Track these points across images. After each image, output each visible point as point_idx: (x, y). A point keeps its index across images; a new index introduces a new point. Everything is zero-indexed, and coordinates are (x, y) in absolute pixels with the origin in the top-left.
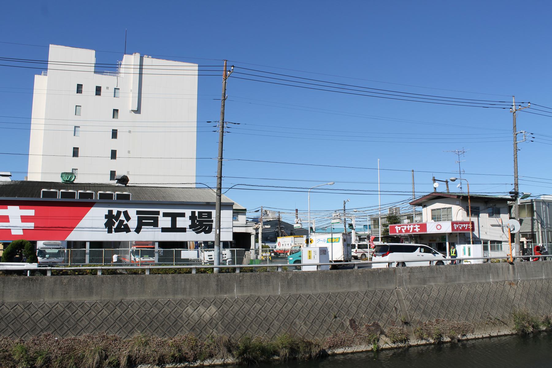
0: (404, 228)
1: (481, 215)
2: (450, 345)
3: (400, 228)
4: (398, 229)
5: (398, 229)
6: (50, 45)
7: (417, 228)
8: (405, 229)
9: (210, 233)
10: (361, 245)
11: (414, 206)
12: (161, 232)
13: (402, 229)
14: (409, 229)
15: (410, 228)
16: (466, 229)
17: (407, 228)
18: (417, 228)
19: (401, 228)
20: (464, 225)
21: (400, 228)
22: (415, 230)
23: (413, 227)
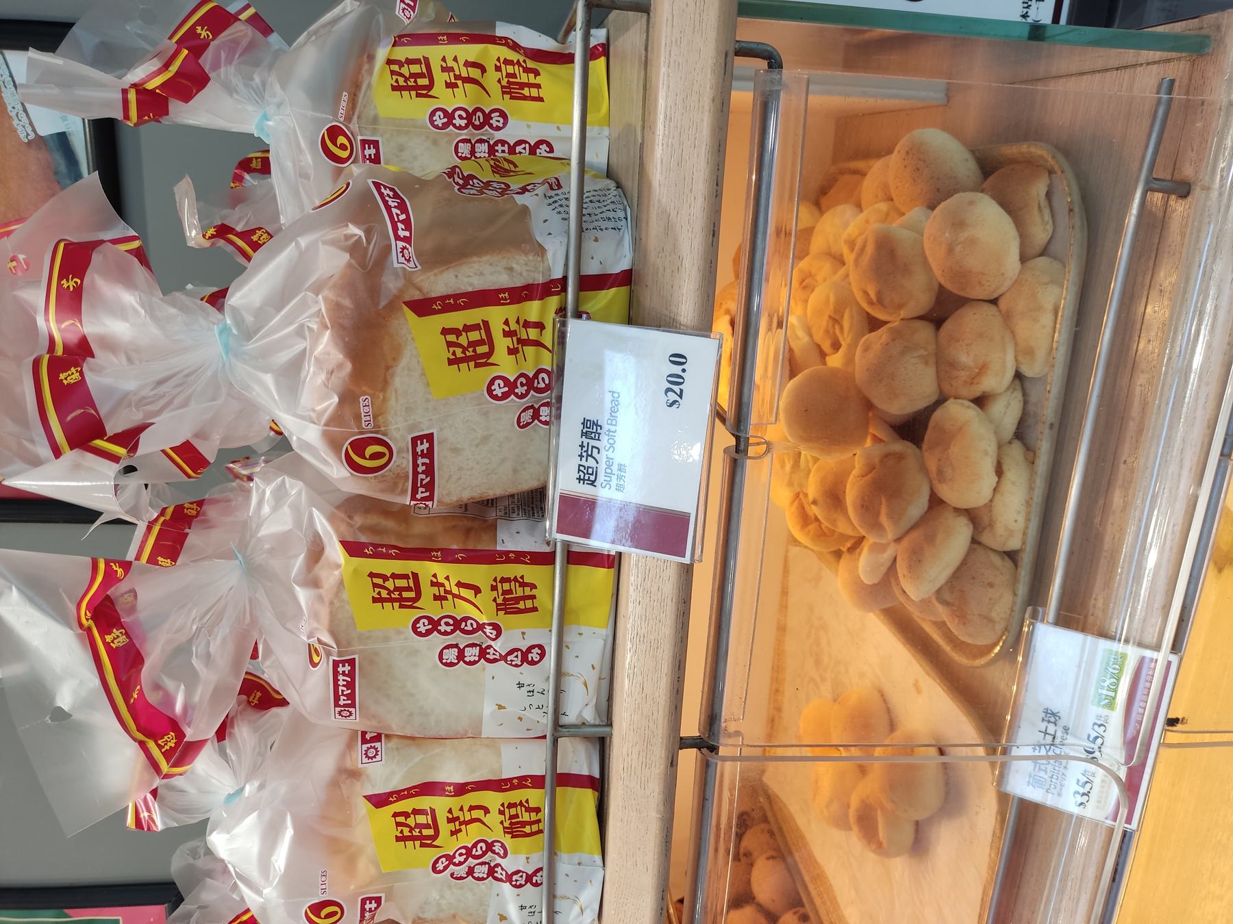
0: (422, 480)
1: (346, 257)
3: (342, 698)
4: (344, 700)
5: (344, 700)
6: (497, 23)
7: (371, 906)
9: (420, 599)
10: (856, 348)
12: (599, 502)
14: (345, 683)
15: (344, 680)
16: (349, 680)
17: (423, 472)
18: (371, 906)
19: (343, 695)
20: (341, 683)
21: (342, 698)
22: (347, 672)
23: (368, 161)
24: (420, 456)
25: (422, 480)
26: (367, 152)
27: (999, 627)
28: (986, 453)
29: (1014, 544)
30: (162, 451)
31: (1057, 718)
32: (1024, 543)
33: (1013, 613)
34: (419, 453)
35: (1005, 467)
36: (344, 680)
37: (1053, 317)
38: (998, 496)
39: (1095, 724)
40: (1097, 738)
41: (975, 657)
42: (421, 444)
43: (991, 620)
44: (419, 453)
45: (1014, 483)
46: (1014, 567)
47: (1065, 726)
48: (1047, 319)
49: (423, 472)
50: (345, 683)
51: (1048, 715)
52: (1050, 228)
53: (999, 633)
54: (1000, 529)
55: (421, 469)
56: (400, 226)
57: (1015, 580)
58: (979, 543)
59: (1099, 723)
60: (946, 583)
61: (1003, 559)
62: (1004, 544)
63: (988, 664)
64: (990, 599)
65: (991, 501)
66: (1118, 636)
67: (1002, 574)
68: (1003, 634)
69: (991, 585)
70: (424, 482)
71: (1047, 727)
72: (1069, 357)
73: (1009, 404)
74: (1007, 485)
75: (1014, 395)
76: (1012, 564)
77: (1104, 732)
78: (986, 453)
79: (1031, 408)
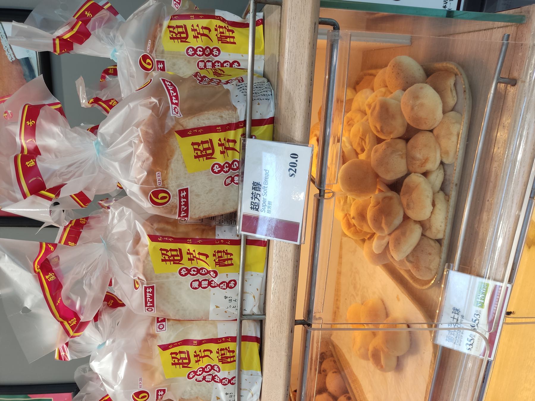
0: (183, 208)
1: (150, 111)
2: (215, 367)
3: (148, 303)
4: (149, 304)
5: (149, 304)
7: (161, 393)
8: (184, 207)
9: (182, 260)
11: (509, 24)
13: (150, 301)
14: (150, 296)
15: (149, 295)
16: (152, 295)
17: (184, 205)
18: (161, 393)
19: (149, 301)
20: (148, 296)
21: (148, 303)
22: (150, 292)
23: (160, 70)
24: (182, 198)
25: (183, 208)
26: (159, 66)
27: (434, 272)
28: (428, 197)
29: (440, 236)
30: (70, 196)
31: (459, 312)
32: (444, 236)
33: (439, 266)
34: (182, 197)
35: (436, 203)
36: (149, 295)
37: (457, 138)
38: (433, 215)
39: (475, 314)
40: (476, 320)
41: (423, 285)
42: (183, 193)
43: (430, 269)
44: (182, 197)
45: (440, 210)
46: (440, 246)
47: (462, 315)
48: (454, 139)
49: (184, 205)
50: (150, 296)
51: (455, 310)
52: (455, 99)
53: (434, 275)
54: (434, 230)
55: (183, 203)
56: (174, 98)
57: (440, 252)
58: (425, 236)
59: (477, 314)
60: (411, 253)
61: (435, 242)
62: (436, 236)
63: (429, 288)
64: (430, 260)
65: (430, 217)
66: (485, 276)
67: (435, 249)
68: (435, 275)
69: (430, 254)
70: (184, 209)
71: (454, 315)
72: (464, 155)
73: (438, 175)
74: (437, 211)
75: (440, 172)
76: (439, 245)
77: (479, 317)
78: (428, 197)
79: (447, 177)
